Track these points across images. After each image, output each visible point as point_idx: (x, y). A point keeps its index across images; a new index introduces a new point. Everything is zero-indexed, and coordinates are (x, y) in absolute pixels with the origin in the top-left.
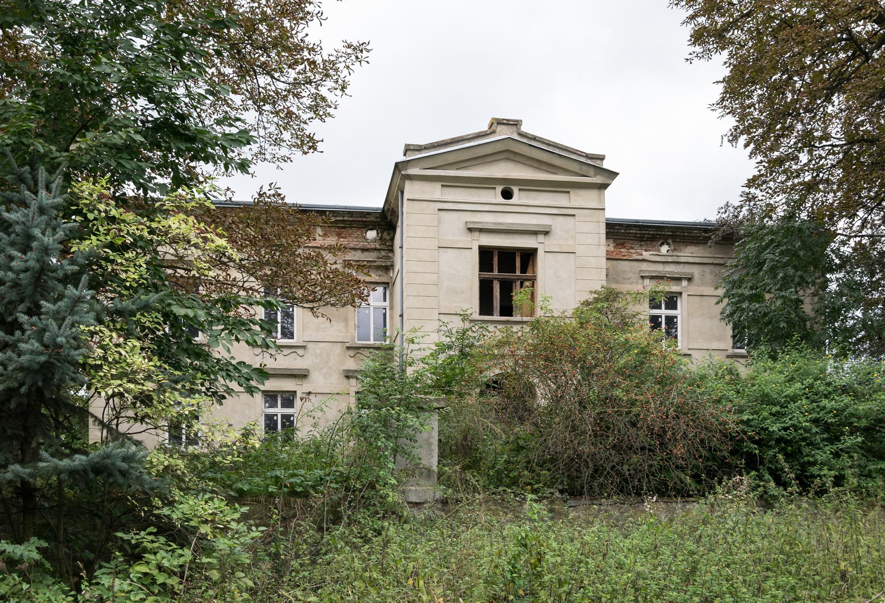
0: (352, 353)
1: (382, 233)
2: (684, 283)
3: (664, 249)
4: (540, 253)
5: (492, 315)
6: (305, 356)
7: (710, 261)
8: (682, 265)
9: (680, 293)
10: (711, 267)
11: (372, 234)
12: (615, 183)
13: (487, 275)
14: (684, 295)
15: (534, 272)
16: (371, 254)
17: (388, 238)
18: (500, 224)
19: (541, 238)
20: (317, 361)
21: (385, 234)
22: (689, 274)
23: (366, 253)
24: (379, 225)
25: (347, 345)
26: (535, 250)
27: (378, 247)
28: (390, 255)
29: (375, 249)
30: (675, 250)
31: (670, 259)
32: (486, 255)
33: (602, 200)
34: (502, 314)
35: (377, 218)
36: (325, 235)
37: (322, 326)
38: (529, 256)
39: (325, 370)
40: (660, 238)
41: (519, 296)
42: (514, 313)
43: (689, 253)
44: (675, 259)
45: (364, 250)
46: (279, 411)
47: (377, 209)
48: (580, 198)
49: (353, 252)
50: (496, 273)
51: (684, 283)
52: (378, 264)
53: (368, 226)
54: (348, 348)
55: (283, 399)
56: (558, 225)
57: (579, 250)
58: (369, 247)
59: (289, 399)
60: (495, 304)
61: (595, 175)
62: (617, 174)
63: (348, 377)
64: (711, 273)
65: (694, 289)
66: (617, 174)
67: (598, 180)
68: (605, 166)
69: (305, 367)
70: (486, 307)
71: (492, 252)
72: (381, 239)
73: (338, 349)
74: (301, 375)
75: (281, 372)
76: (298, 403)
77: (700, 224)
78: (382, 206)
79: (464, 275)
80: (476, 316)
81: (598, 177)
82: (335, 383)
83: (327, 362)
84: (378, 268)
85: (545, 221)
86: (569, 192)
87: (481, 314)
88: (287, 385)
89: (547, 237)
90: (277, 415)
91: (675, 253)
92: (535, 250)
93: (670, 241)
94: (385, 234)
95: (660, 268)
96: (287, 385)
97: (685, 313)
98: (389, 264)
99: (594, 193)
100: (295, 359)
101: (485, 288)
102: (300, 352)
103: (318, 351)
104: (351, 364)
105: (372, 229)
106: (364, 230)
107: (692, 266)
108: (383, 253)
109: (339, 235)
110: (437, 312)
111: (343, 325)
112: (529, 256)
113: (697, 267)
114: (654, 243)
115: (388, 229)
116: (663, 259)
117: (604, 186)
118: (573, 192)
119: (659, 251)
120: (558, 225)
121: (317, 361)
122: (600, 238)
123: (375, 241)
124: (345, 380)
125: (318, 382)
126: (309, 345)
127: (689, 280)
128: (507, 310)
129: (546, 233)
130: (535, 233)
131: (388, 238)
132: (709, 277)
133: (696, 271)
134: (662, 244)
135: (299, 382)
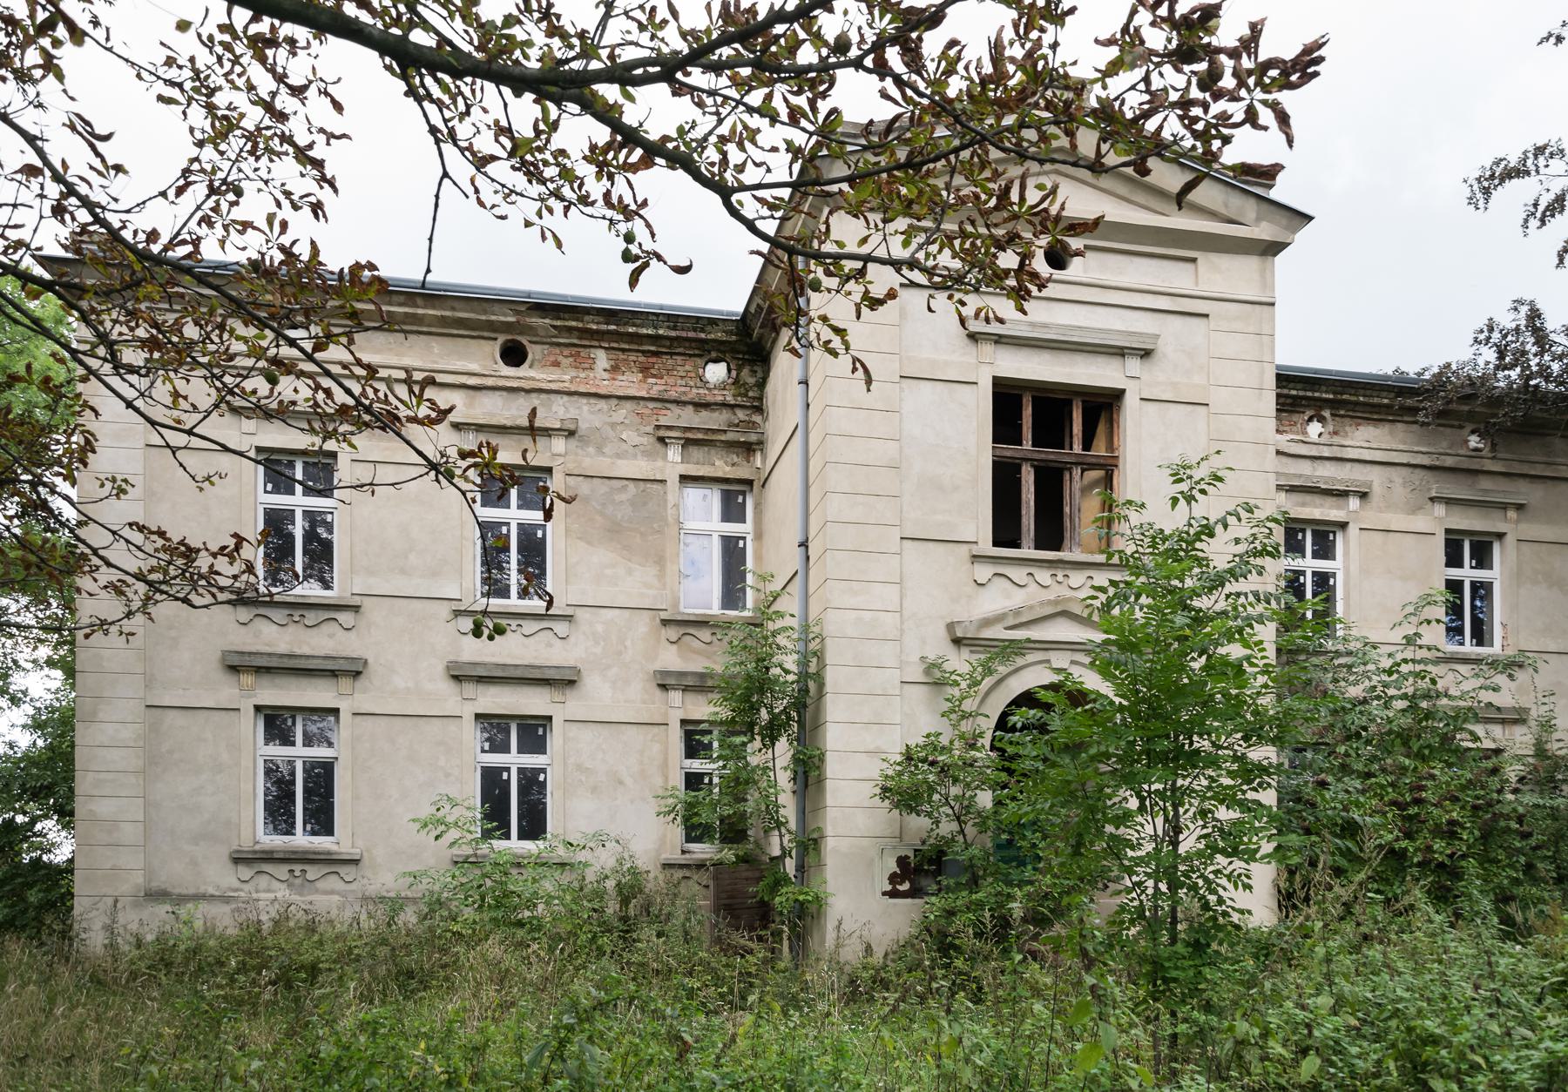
0: (673, 633)
1: (739, 370)
2: (1354, 503)
3: (1315, 429)
4: (1130, 402)
5: (1018, 546)
6: (572, 639)
7: (1404, 458)
8: (1349, 465)
9: (1343, 526)
10: (1405, 471)
11: (716, 372)
12: (1303, 238)
13: (1009, 450)
14: (1353, 530)
15: (1111, 446)
16: (716, 414)
17: (751, 381)
18: (1045, 326)
19: (1133, 365)
20: (598, 650)
21: (745, 372)
22: (1364, 483)
23: (704, 413)
24: (734, 351)
25: (664, 615)
26: (1118, 395)
27: (730, 399)
28: (757, 418)
29: (724, 405)
30: (1335, 433)
31: (1326, 452)
32: (1007, 396)
33: (1267, 281)
34: (1039, 546)
35: (731, 333)
36: (615, 369)
37: (608, 572)
38: (1102, 406)
39: (614, 670)
40: (1308, 406)
41: (1083, 508)
42: (1067, 542)
43: (1365, 439)
44: (1338, 452)
45: (700, 405)
46: (514, 760)
47: (733, 314)
48: (1223, 275)
49: (676, 410)
50: (1027, 444)
51: (1354, 503)
52: (730, 436)
53: (708, 351)
54: (665, 622)
55: (522, 729)
56: (1171, 335)
57: (1218, 398)
58: (710, 399)
59: (534, 733)
60: (1024, 520)
61: (1258, 220)
62: (1310, 218)
63: (663, 687)
64: (1404, 485)
65: (1372, 515)
66: (1310, 218)
67: (1264, 231)
68: (1274, 194)
69: (571, 663)
70: (1006, 532)
71: (1019, 398)
72: (736, 382)
73: (643, 624)
74: (563, 682)
75: (518, 673)
76: (555, 740)
77: (1386, 377)
78: (741, 309)
79: (963, 442)
80: (986, 546)
81: (1264, 224)
82: (638, 699)
83: (620, 653)
84: (731, 445)
85: (1142, 325)
86: (1194, 260)
87: (996, 544)
88: (532, 702)
89: (1147, 363)
90: (508, 770)
91: (1336, 440)
92: (1118, 395)
93: (1327, 414)
94: (745, 372)
95: (1305, 468)
96: (532, 702)
97: (1354, 568)
98: (753, 438)
99: (1250, 263)
100: (550, 645)
101: (1005, 478)
102: (345, 618)
103: (600, 628)
104: (671, 659)
105: (716, 361)
106: (700, 361)
107: (1369, 467)
108: (741, 415)
109: (645, 370)
110: (896, 534)
111: (652, 571)
112: (1102, 406)
113: (1377, 468)
114: (1295, 417)
115: (752, 362)
116: (1314, 451)
117: (1273, 248)
118: (1206, 260)
119: (1305, 433)
120: (1171, 335)
121: (598, 650)
122: (1262, 372)
123: (722, 386)
124: (658, 692)
125: (600, 694)
126: (580, 614)
127: (1364, 496)
128: (1052, 533)
129: (1146, 354)
130: (1120, 352)
131: (751, 381)
132: (1400, 492)
133: (1375, 478)
134: (1310, 419)
135: (558, 697)
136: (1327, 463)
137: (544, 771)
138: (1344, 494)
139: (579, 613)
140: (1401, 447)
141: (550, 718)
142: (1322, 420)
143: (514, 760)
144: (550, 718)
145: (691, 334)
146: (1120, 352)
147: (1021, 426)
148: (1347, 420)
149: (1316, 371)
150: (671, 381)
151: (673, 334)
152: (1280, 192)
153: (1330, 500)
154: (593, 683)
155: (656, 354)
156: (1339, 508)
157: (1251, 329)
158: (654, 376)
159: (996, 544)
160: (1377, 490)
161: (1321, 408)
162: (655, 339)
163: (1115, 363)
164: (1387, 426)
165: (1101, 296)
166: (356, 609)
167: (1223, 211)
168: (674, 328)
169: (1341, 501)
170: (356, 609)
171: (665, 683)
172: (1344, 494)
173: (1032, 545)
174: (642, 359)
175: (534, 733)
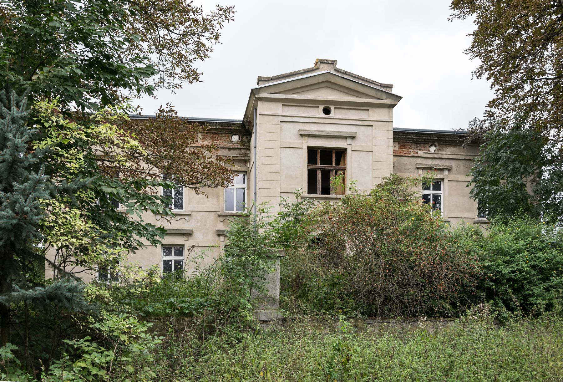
1: (242, 137)
2: (446, 172)
3: (432, 149)
4: (349, 151)
5: (316, 193)
6: (191, 221)
7: (463, 157)
9: (443, 180)
10: (464, 162)
11: (235, 138)
12: (400, 104)
13: (313, 166)
14: (446, 181)
16: (235, 151)
17: (246, 140)
18: (322, 131)
19: (349, 141)
20: (198, 224)
21: (244, 138)
22: (449, 166)
23: (232, 151)
25: (219, 213)
26: (346, 149)
27: (239, 147)
28: (248, 152)
29: (238, 148)
30: (440, 150)
31: (436, 156)
32: (312, 151)
33: (391, 115)
36: (204, 139)
37: (202, 200)
38: (341, 153)
40: (430, 142)
43: (449, 152)
44: (440, 156)
45: (230, 149)
46: (173, 258)
49: (223, 150)
50: (319, 165)
51: (446, 172)
52: (239, 158)
54: (219, 216)
55: (175, 250)
57: (375, 149)
58: (233, 147)
59: (179, 250)
60: (318, 186)
61: (386, 98)
63: (219, 235)
64: (464, 166)
65: (452, 177)
66: (401, 98)
67: (388, 101)
70: (312, 188)
71: (317, 151)
72: (241, 141)
73: (213, 216)
74: (188, 234)
75: (174, 232)
76: (185, 252)
78: (241, 118)
79: (299, 164)
80: (306, 194)
81: (388, 99)
84: (240, 161)
86: (368, 110)
87: (309, 193)
89: (354, 141)
90: (171, 261)
91: (440, 152)
92: (346, 149)
93: (436, 144)
94: (244, 138)
95: (429, 162)
97: (446, 193)
98: (247, 158)
99: (385, 110)
101: (312, 175)
103: (199, 218)
104: (221, 227)
105: (235, 135)
106: (230, 135)
108: (243, 151)
109: (213, 139)
110: (279, 191)
112: (341, 153)
114: (426, 145)
115: (246, 135)
116: (432, 156)
117: (392, 106)
119: (429, 150)
120: (360, 132)
121: (198, 224)
123: (237, 142)
124: (217, 238)
125: (199, 238)
127: (449, 170)
128: (326, 190)
129: (353, 138)
130: (345, 138)
131: (246, 140)
132: (462, 168)
133: (453, 164)
134: (431, 146)
135: (186, 239)
136: (437, 160)
137: (182, 261)
138: (442, 170)
139: (193, 213)
140: (460, 154)
141: (184, 245)
142: (435, 146)
143: (173, 258)
144: (184, 245)
145: (227, 128)
146: (345, 138)
147: (317, 159)
148: (444, 146)
149: (431, 131)
150: (221, 142)
151: (222, 128)
152: (394, 91)
153: (438, 172)
154: (196, 234)
155: (217, 134)
156: (441, 174)
157: (386, 129)
158: (216, 140)
159: (309, 193)
160: (454, 168)
161: (434, 142)
162: (216, 129)
163: (344, 141)
164: (458, 147)
165: (339, 122)
166: (189, 215)
167: (376, 96)
168: (222, 126)
169: (442, 172)
170: (189, 215)
171: (219, 234)
172: (442, 170)
173: (321, 193)
174: (212, 135)
175: (179, 250)
